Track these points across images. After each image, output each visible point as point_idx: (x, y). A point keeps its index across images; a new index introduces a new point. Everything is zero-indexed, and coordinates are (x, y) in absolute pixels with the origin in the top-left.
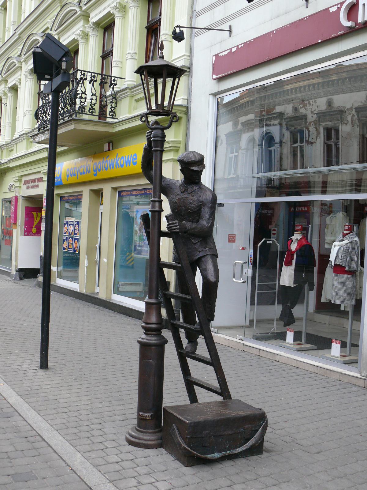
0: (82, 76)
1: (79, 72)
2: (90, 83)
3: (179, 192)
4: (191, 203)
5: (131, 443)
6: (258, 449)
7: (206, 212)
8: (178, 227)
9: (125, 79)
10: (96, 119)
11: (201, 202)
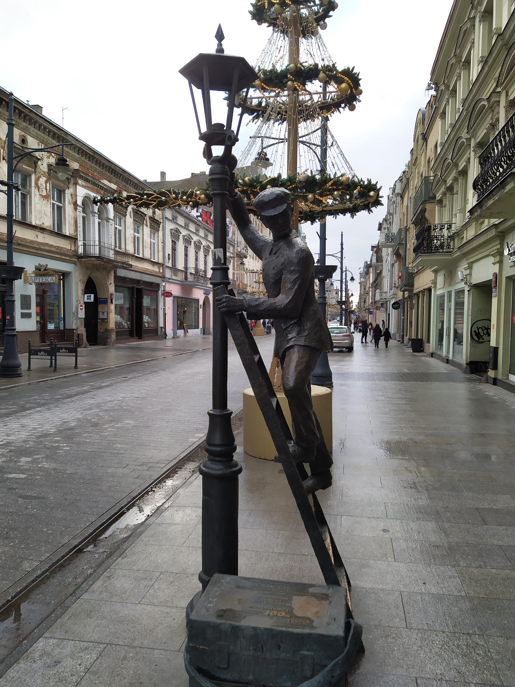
8: (225, 304)
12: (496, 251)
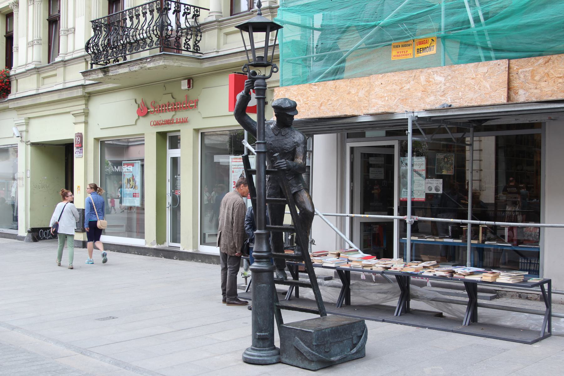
0: (186, 11)
1: (182, 6)
2: (173, 14)
3: (273, 135)
4: (286, 144)
5: (248, 361)
6: (360, 355)
7: (300, 150)
9: (209, 10)
10: (157, 51)
11: (295, 143)
12: (82, 111)
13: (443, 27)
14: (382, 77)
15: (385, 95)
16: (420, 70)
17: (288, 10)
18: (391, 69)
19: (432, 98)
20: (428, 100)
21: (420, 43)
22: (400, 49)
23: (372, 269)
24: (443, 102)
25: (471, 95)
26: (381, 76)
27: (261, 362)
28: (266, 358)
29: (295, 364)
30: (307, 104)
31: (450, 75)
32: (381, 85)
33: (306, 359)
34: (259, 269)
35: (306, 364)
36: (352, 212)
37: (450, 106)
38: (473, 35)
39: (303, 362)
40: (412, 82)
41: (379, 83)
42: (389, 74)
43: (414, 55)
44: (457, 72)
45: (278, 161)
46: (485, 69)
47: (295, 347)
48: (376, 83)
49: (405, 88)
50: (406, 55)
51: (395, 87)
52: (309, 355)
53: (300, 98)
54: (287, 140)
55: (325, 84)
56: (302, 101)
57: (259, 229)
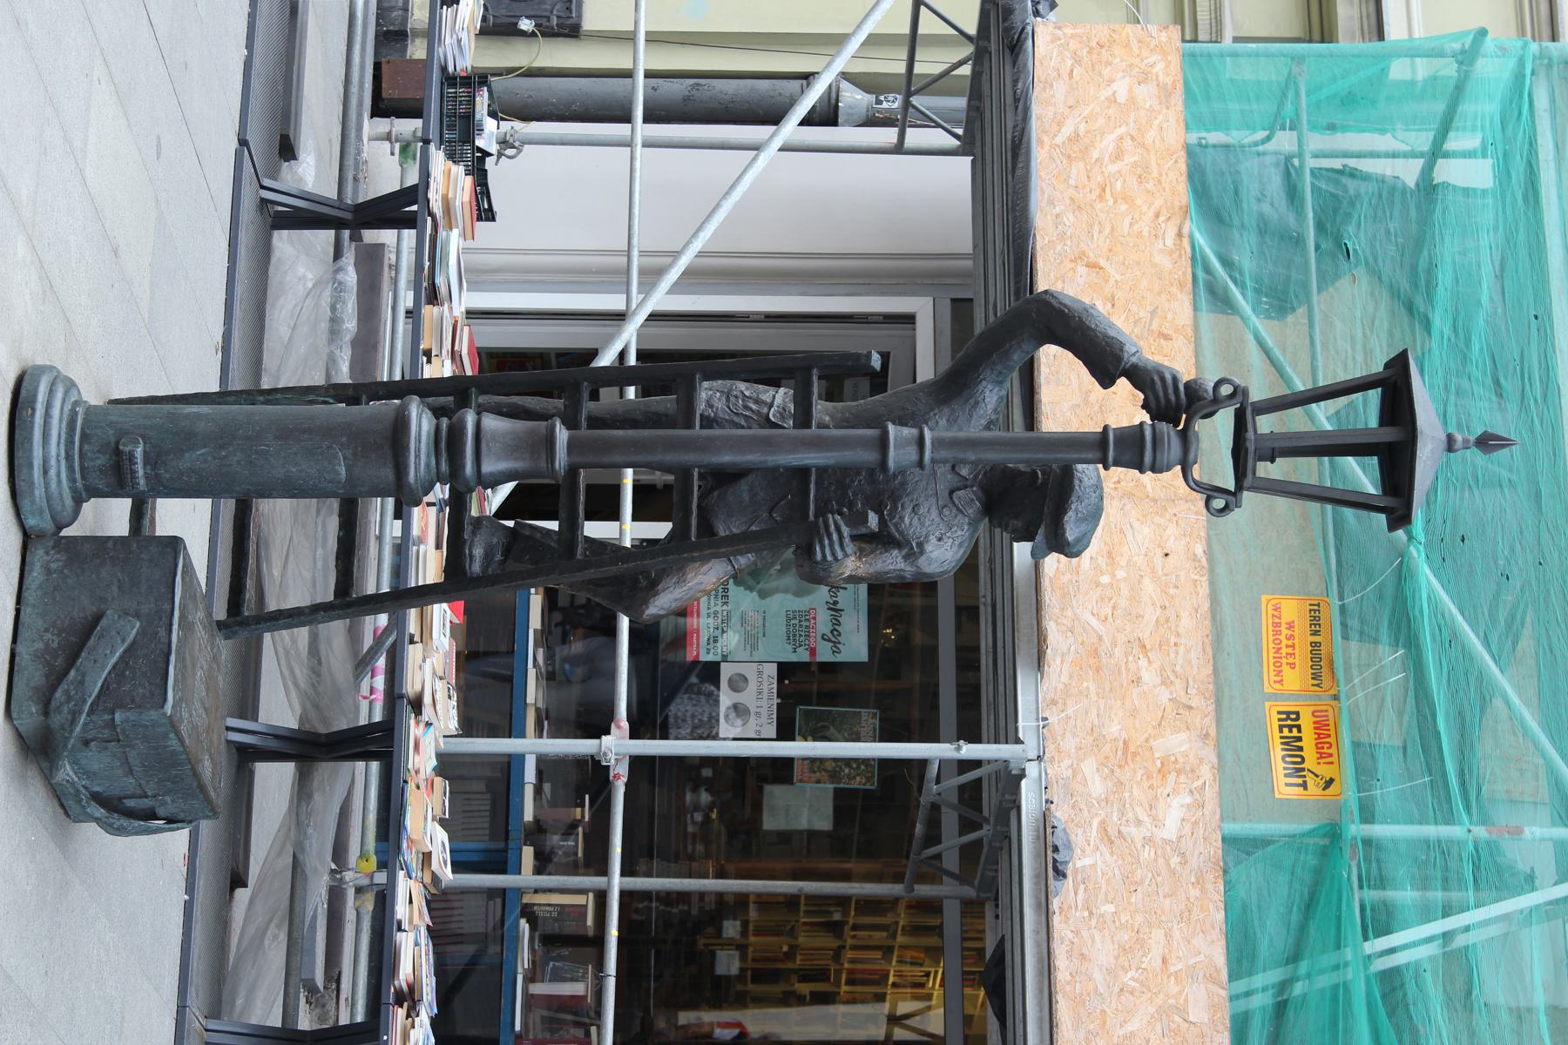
11: (920, 545)
13: (1379, 830)
14: (1195, 559)
15: (1121, 574)
16: (1213, 732)
17: (1519, 77)
18: (1225, 600)
19: (1097, 787)
20: (1089, 767)
21: (1321, 727)
22: (1303, 637)
23: (412, 642)
24: (1078, 838)
25: (1103, 952)
26: (1199, 549)
27: (21, 476)
28: (39, 492)
29: (27, 611)
30: (1101, 197)
31: (1184, 863)
32: (1160, 553)
33: (56, 678)
34: (406, 458)
35: (33, 674)
36: (649, 75)
37: (1060, 874)
38: (1338, 947)
39: (37, 656)
40: (1164, 696)
41: (1170, 545)
42: (1204, 589)
43: (1274, 697)
44: (1194, 893)
45: (846, 531)
46: (1198, 1014)
47: (97, 618)
48: (1172, 530)
49: (1143, 662)
50: (1278, 664)
51: (1151, 615)
52: (69, 699)
53: (1130, 159)
54: (934, 514)
55: (1181, 285)
56: (1113, 168)
57: (572, 446)
